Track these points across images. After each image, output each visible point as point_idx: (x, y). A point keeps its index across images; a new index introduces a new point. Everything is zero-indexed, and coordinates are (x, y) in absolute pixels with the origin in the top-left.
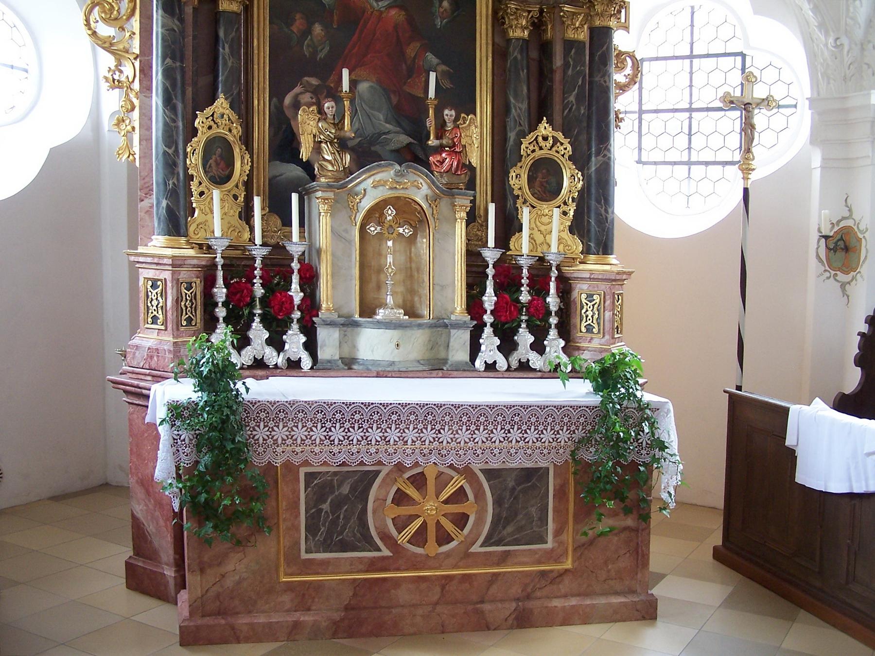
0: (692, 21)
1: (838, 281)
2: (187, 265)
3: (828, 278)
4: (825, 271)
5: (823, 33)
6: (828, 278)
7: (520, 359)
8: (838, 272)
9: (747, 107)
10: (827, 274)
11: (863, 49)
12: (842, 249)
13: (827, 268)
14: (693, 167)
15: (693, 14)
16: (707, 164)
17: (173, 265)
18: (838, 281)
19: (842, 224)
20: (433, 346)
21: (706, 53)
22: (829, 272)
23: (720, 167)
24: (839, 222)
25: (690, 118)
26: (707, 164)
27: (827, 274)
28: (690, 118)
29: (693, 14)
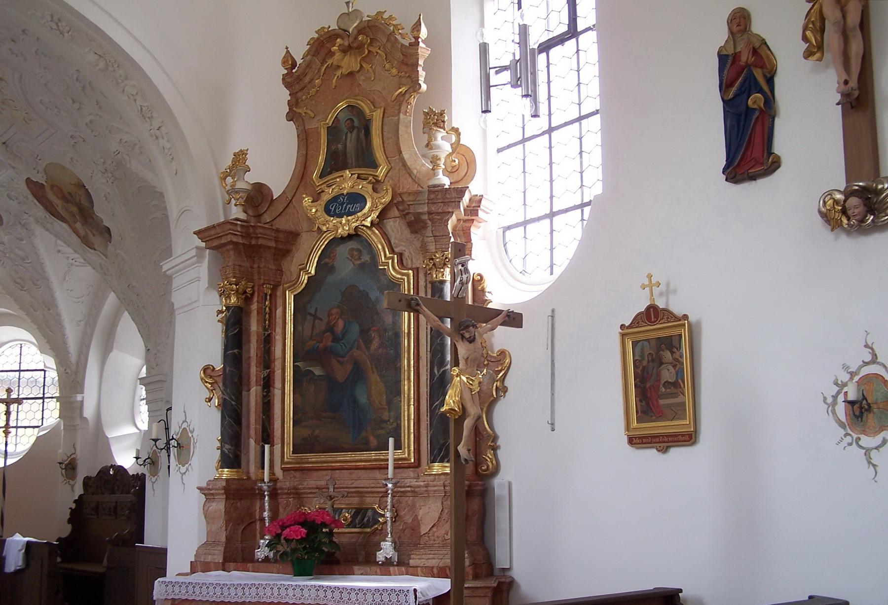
0: (21, 352)
1: (70, 484)
2: (383, 231)
3: (850, 444)
4: (846, 435)
5: (806, 20)
6: (66, 483)
7: (116, 518)
8: (70, 480)
9: (43, 398)
10: (65, 482)
11: (76, 374)
12: (71, 469)
13: (66, 479)
14: (19, 429)
15: (21, 347)
16: (25, 427)
17: (736, 54)
18: (70, 484)
19: (72, 457)
20: (276, 485)
21: (548, 117)
22: (850, 435)
23: (32, 429)
24: (71, 455)
25: (44, 394)
26: (25, 427)
27: (849, 439)
28: (44, 394)
29: (21, 347)
